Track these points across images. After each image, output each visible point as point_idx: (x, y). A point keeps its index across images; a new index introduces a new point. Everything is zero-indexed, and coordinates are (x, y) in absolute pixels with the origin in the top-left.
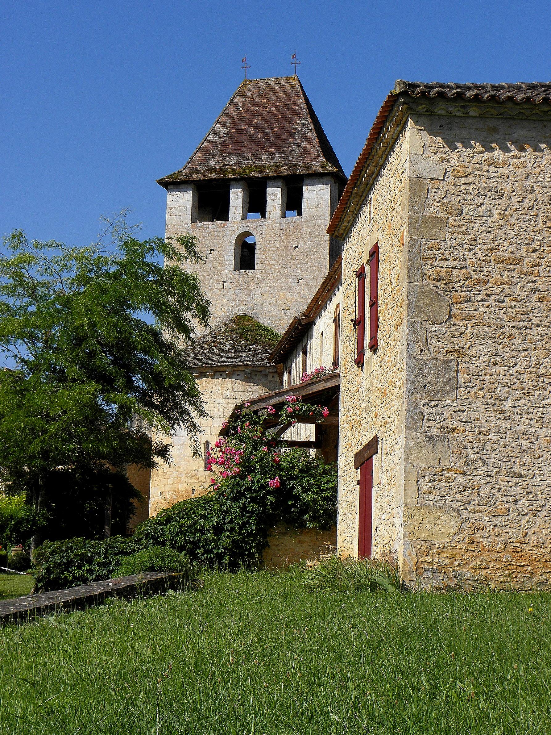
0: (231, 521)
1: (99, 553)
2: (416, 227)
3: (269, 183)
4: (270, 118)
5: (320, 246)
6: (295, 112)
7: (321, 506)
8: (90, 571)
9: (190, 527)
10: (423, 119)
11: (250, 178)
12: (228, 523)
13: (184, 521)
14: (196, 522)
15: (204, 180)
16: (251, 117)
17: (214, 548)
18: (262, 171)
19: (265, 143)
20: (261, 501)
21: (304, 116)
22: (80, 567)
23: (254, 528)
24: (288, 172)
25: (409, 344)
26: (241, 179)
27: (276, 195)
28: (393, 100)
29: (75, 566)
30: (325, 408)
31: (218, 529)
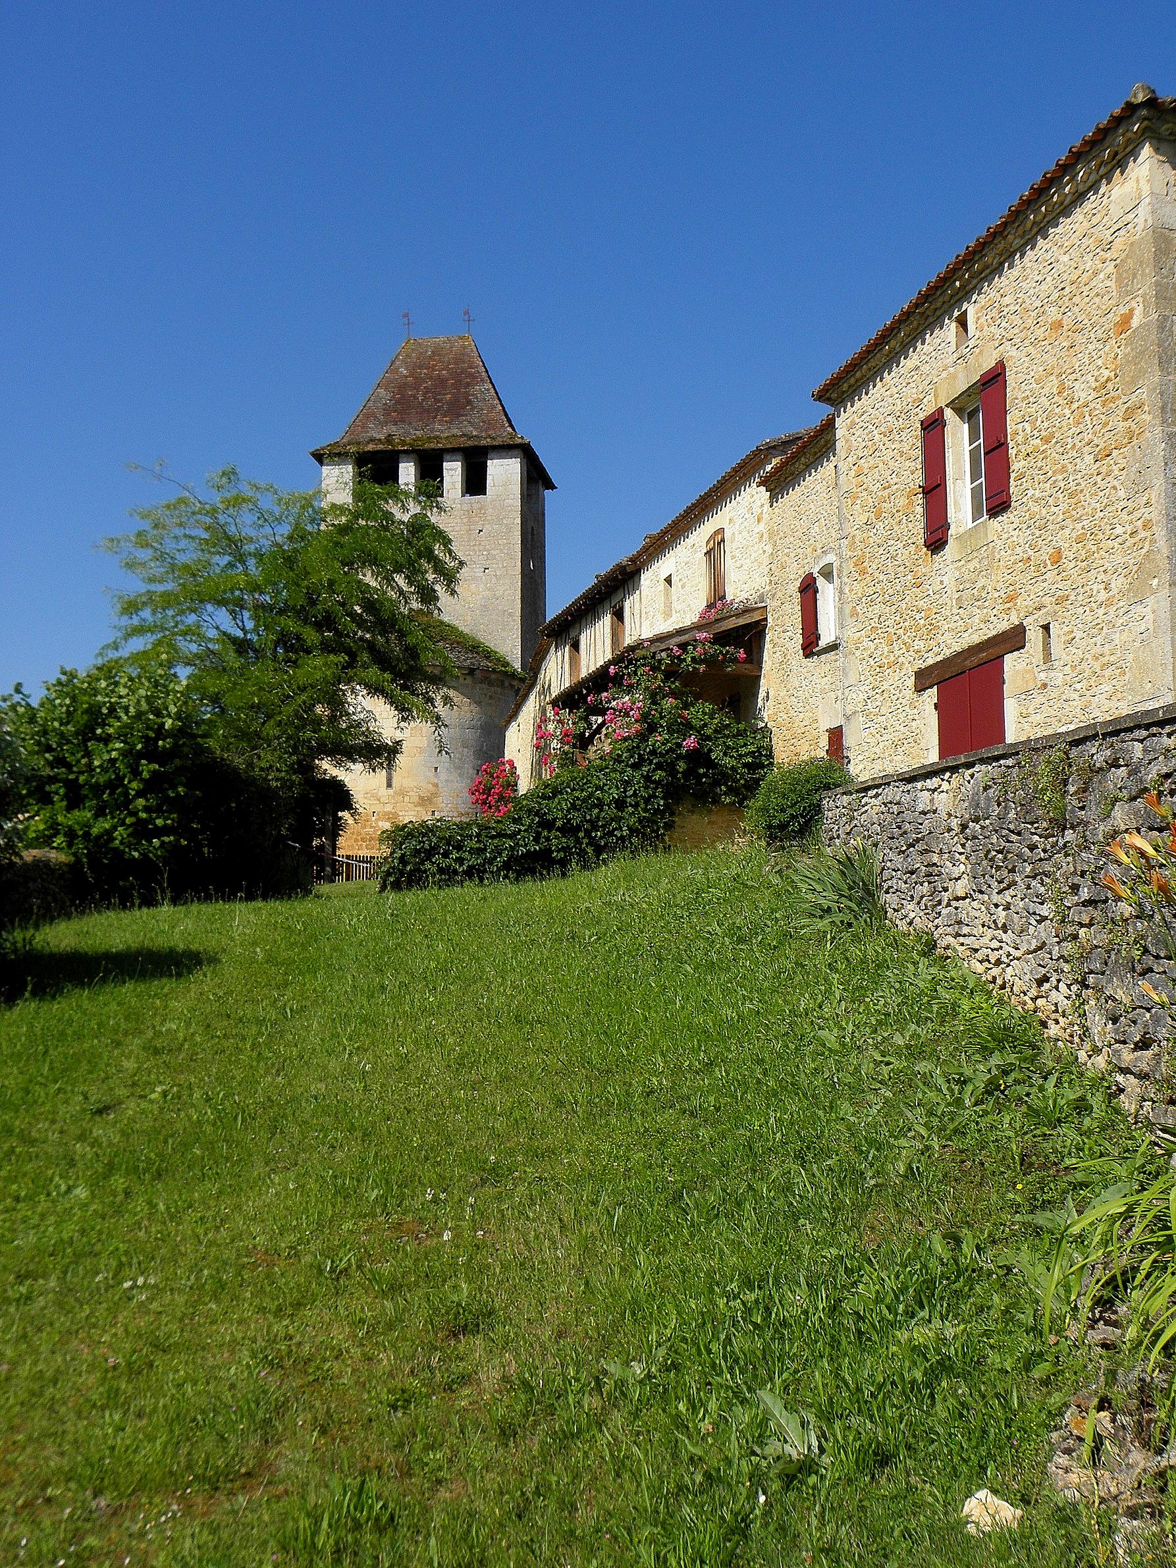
0: (635, 794)
1: (471, 836)
2: (1165, 298)
3: (446, 457)
4: (441, 382)
5: (509, 530)
6: (472, 376)
7: (742, 775)
8: (460, 860)
9: (584, 800)
10: (1165, 147)
11: (423, 450)
12: (630, 797)
13: (577, 794)
14: (591, 795)
15: (369, 451)
16: (418, 381)
17: (616, 829)
18: (438, 442)
19: (438, 410)
20: (671, 769)
21: (482, 380)
22: (446, 855)
23: (662, 802)
24: (470, 443)
25: (1166, 464)
26: (414, 451)
27: (455, 470)
28: (1131, 109)
29: (438, 854)
30: (742, 650)
31: (620, 804)
